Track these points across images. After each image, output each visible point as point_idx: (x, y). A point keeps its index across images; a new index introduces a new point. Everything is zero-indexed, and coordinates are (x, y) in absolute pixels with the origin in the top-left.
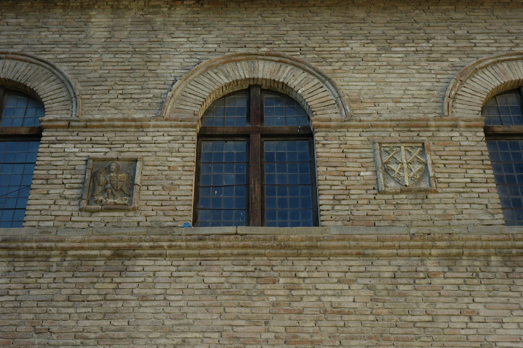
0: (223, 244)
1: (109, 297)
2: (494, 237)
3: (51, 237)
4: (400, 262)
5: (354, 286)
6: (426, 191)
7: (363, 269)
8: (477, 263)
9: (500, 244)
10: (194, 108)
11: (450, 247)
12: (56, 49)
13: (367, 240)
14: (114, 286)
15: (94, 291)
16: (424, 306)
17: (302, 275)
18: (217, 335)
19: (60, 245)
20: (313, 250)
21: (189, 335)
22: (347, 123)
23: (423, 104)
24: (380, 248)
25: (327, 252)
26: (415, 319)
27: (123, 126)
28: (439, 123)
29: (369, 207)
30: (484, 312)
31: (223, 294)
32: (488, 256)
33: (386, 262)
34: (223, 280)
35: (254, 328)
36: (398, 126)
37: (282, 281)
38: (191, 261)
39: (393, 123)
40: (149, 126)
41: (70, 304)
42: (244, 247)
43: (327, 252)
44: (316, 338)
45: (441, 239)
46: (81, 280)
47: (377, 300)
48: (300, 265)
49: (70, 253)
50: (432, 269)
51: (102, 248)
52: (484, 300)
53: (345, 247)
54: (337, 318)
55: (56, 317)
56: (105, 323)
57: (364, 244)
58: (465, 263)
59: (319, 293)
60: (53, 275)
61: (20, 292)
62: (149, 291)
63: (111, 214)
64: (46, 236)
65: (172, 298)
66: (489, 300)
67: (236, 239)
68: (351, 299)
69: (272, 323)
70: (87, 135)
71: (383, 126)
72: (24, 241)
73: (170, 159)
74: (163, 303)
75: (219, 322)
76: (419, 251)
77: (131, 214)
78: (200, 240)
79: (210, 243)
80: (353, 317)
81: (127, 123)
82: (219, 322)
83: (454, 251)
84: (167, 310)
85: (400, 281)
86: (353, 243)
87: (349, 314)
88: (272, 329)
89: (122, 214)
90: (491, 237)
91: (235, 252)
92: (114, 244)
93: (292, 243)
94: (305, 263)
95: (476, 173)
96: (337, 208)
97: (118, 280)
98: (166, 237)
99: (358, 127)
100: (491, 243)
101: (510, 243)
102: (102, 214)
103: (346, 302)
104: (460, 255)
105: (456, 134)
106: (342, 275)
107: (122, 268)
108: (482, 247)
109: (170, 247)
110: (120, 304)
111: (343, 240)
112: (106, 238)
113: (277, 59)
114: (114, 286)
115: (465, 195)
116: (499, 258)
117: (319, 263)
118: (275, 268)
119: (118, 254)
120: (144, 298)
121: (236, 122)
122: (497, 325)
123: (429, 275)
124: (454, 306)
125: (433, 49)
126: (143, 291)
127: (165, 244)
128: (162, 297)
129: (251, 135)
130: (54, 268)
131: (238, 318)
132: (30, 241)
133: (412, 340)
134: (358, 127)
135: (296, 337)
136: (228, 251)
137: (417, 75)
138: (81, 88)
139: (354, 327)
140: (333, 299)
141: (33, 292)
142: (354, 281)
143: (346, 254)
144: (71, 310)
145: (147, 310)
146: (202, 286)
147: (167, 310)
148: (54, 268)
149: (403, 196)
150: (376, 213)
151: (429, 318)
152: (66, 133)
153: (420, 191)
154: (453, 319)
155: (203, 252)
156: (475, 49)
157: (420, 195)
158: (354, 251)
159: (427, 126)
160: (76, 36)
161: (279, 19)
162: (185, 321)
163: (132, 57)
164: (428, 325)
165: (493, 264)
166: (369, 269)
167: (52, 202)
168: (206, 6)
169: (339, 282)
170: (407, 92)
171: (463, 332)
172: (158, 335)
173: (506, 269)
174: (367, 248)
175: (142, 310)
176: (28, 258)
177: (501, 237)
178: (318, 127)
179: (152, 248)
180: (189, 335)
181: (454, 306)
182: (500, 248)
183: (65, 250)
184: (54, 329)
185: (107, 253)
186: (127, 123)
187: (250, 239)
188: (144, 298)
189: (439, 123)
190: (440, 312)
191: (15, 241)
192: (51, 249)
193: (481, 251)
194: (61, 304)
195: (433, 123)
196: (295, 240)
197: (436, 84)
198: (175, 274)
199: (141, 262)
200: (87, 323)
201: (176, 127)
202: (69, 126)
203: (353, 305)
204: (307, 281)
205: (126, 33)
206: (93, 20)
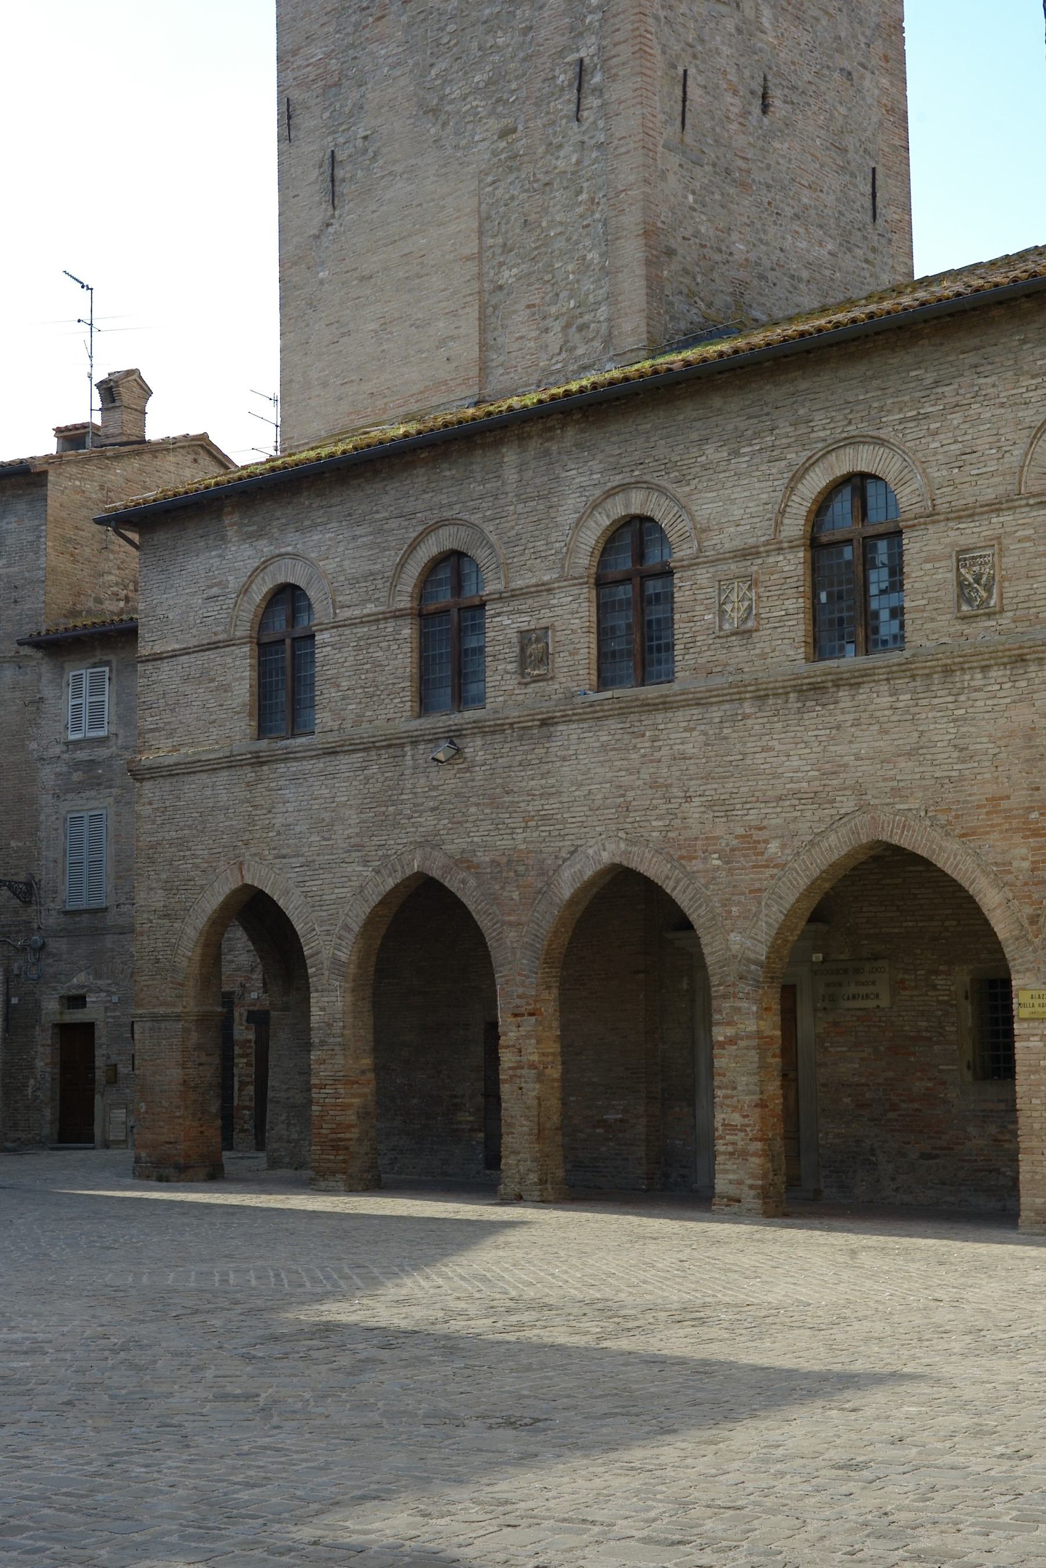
0: (606, 708)
1: (544, 760)
2: (788, 677)
3: (500, 716)
4: (727, 706)
5: (695, 733)
6: (750, 631)
7: (700, 717)
8: (779, 701)
9: (792, 683)
10: (584, 561)
11: (758, 690)
12: (484, 505)
13: (700, 692)
14: (545, 750)
15: (534, 756)
16: (738, 746)
17: (661, 727)
18: (608, 785)
19: (507, 721)
20: (665, 705)
21: (592, 787)
22: (696, 561)
23: (758, 525)
24: (710, 697)
25: (675, 705)
26: (732, 758)
27: (537, 592)
28: (767, 548)
29: (709, 653)
30: (778, 747)
31: (611, 750)
32: (788, 693)
33: (716, 709)
34: (610, 737)
35: (632, 777)
36: (735, 556)
37: (648, 734)
38: (591, 723)
39: (731, 555)
40: (554, 589)
41: (521, 768)
42: (620, 708)
43: (675, 705)
44: (669, 781)
45: (750, 685)
46: (526, 747)
47: (708, 745)
48: (660, 717)
49: (515, 726)
50: (748, 711)
51: (533, 720)
52: (779, 737)
53: (686, 700)
54: (682, 762)
55: (515, 779)
56: (543, 782)
57: (698, 695)
58: (770, 702)
59: (671, 742)
60: (509, 745)
61: (493, 761)
62: (565, 752)
63: (539, 684)
64: (497, 716)
65: (581, 757)
66: (783, 735)
67: (613, 703)
68: (691, 745)
69: (642, 770)
70: (515, 604)
71: (724, 559)
72: (485, 721)
73: (572, 621)
74: (575, 762)
75: (610, 774)
76: (737, 697)
77: (550, 683)
78: (591, 706)
79: (598, 708)
80: (692, 761)
81: (539, 588)
82: (610, 774)
83: (762, 693)
84: (579, 767)
85: (725, 725)
86: (691, 696)
87: (690, 758)
88: (642, 776)
89: (545, 683)
90: (785, 678)
91: (616, 712)
92: (539, 717)
93: (650, 701)
94: (662, 715)
95: (791, 605)
96: (687, 657)
97: (547, 745)
98: (569, 707)
99: (706, 563)
100: (786, 684)
101: (799, 682)
102: (532, 685)
103: (689, 749)
104: (767, 695)
105: (781, 558)
106: (686, 724)
107: (548, 734)
108: (780, 688)
109: (574, 714)
110: (550, 765)
111: (684, 694)
112: (532, 712)
113: (645, 486)
114: (545, 750)
115: (779, 630)
116: (796, 695)
117: (671, 715)
118: (644, 723)
119: (544, 723)
120: (564, 759)
121: (625, 563)
122: (785, 758)
123: (746, 717)
124: (759, 744)
125: (776, 443)
126: (563, 753)
127: (570, 712)
128: (574, 757)
129: (226, 988)
130: (509, 740)
131: (620, 770)
132: (489, 720)
133: (728, 777)
134: (706, 563)
135: (656, 782)
136: (611, 713)
137: (757, 485)
138: (505, 551)
139: (693, 770)
140: (680, 747)
141: (500, 760)
142: (694, 729)
143: (688, 705)
144: (523, 774)
145: (567, 769)
146: (598, 744)
147: (579, 767)
148: (509, 740)
149: (734, 638)
150: (714, 658)
151: (740, 757)
152: (501, 605)
153: (745, 632)
154: (757, 756)
155: (596, 715)
156: (812, 435)
157: (746, 635)
158: (693, 702)
159: (758, 553)
160: (494, 484)
161: (649, 426)
162: (589, 776)
163: (538, 504)
164: (740, 763)
165: (791, 700)
166: (706, 716)
167: (499, 678)
168: (591, 419)
169: (685, 731)
170: (748, 511)
171: (762, 767)
172: (574, 788)
173: (799, 705)
174: (702, 698)
175: (564, 769)
176: (493, 732)
177: (792, 677)
178: (676, 568)
179: (563, 716)
180: (592, 787)
181: (759, 744)
182: (795, 686)
183: (512, 724)
184: (516, 789)
185: (537, 723)
186: (539, 588)
187: (623, 702)
188: (564, 759)
189: (767, 548)
190: (748, 751)
191: (480, 722)
192: (503, 725)
193: (780, 691)
194: (517, 769)
195: (762, 549)
196: (652, 699)
197: (772, 494)
198: (581, 736)
199: (560, 728)
200: (532, 783)
201: (574, 585)
202: (501, 598)
203: (693, 751)
204: (664, 732)
205: (531, 472)
206: (506, 460)
